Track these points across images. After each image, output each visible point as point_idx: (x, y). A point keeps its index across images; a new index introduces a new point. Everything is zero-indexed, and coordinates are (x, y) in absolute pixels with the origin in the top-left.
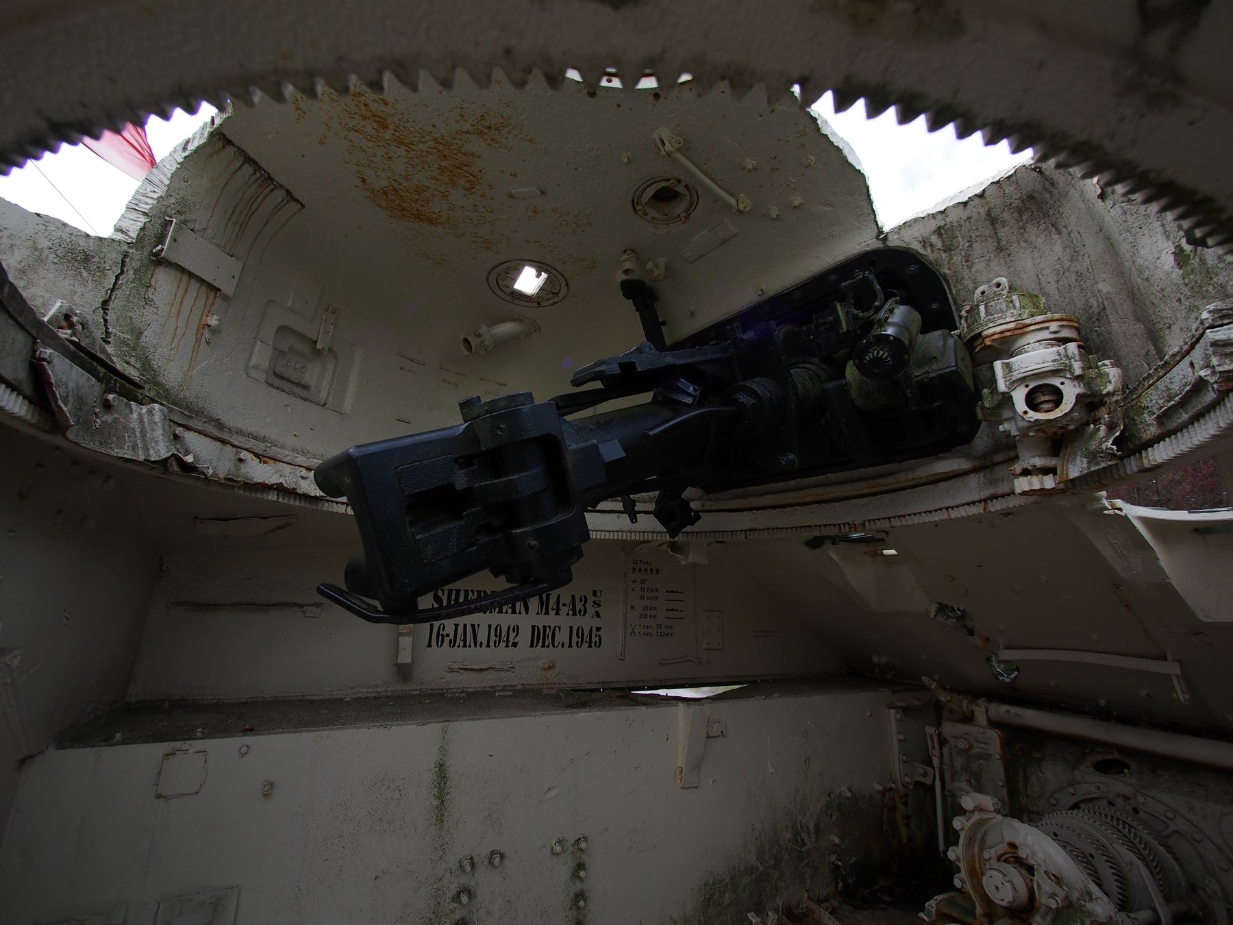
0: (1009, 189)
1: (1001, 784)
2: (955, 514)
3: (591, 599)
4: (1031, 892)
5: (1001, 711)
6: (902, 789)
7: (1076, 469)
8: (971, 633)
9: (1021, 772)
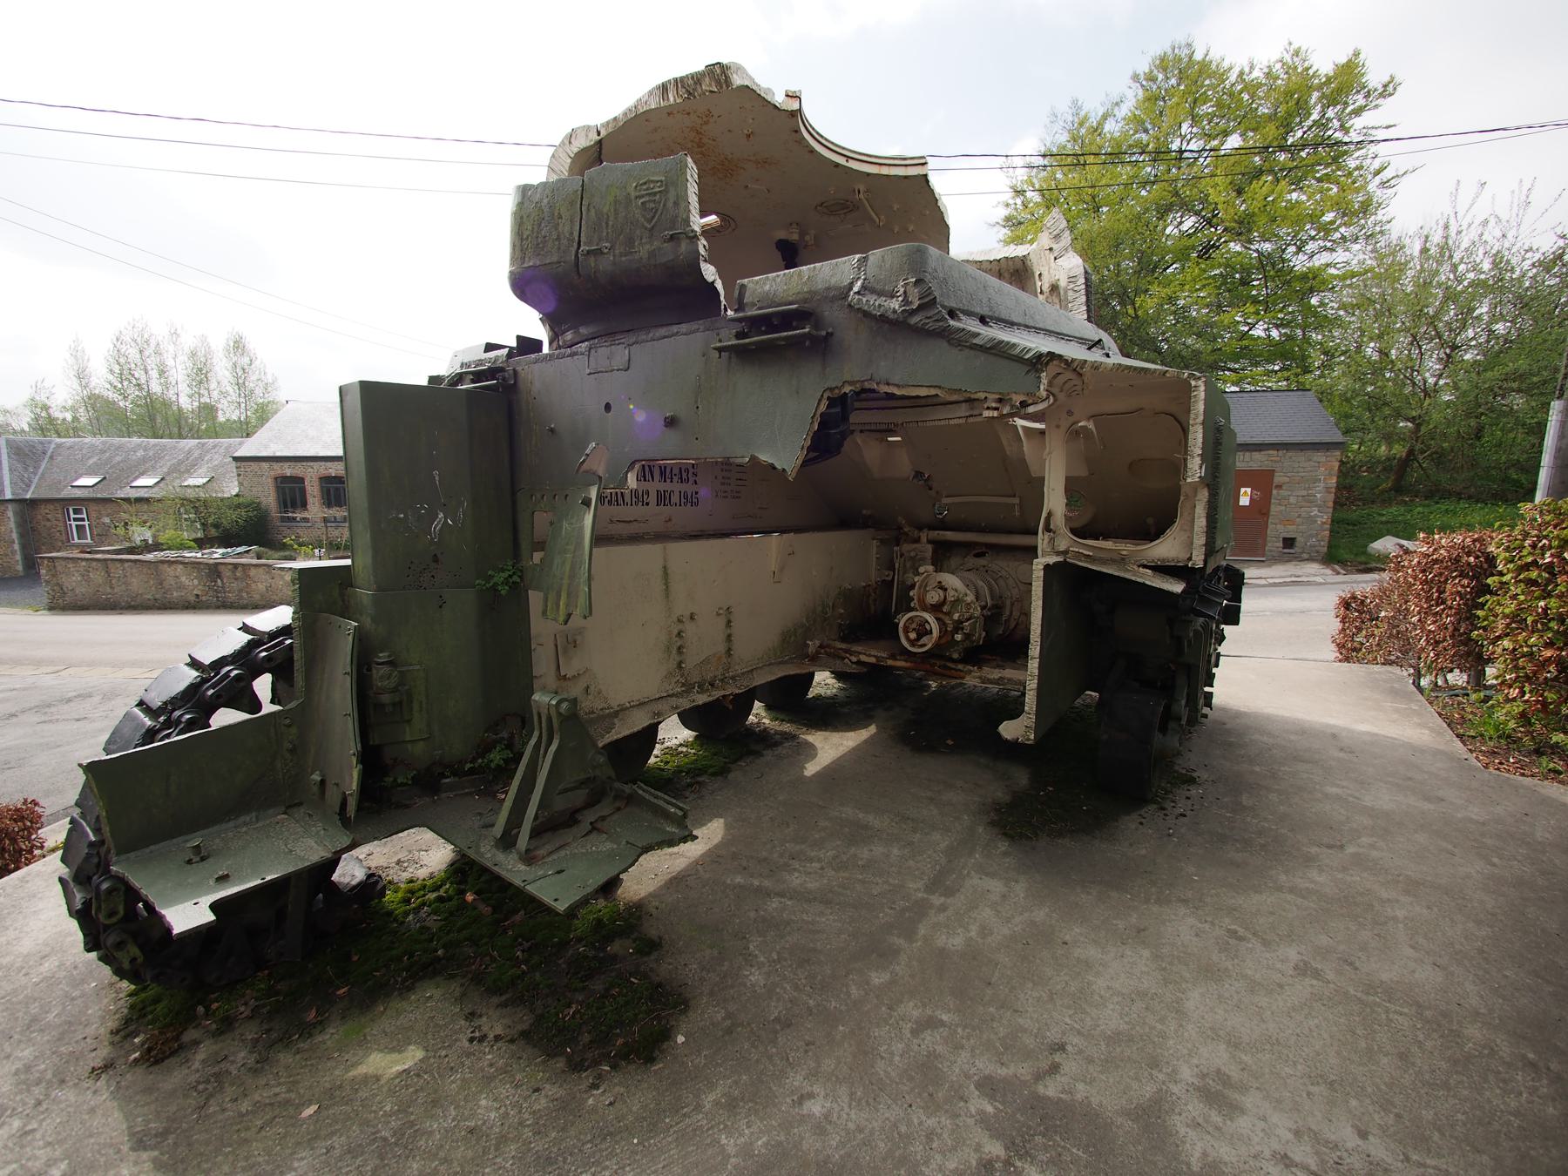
0: (1011, 263)
2: (951, 422)
3: (691, 470)
4: (945, 597)
5: (935, 534)
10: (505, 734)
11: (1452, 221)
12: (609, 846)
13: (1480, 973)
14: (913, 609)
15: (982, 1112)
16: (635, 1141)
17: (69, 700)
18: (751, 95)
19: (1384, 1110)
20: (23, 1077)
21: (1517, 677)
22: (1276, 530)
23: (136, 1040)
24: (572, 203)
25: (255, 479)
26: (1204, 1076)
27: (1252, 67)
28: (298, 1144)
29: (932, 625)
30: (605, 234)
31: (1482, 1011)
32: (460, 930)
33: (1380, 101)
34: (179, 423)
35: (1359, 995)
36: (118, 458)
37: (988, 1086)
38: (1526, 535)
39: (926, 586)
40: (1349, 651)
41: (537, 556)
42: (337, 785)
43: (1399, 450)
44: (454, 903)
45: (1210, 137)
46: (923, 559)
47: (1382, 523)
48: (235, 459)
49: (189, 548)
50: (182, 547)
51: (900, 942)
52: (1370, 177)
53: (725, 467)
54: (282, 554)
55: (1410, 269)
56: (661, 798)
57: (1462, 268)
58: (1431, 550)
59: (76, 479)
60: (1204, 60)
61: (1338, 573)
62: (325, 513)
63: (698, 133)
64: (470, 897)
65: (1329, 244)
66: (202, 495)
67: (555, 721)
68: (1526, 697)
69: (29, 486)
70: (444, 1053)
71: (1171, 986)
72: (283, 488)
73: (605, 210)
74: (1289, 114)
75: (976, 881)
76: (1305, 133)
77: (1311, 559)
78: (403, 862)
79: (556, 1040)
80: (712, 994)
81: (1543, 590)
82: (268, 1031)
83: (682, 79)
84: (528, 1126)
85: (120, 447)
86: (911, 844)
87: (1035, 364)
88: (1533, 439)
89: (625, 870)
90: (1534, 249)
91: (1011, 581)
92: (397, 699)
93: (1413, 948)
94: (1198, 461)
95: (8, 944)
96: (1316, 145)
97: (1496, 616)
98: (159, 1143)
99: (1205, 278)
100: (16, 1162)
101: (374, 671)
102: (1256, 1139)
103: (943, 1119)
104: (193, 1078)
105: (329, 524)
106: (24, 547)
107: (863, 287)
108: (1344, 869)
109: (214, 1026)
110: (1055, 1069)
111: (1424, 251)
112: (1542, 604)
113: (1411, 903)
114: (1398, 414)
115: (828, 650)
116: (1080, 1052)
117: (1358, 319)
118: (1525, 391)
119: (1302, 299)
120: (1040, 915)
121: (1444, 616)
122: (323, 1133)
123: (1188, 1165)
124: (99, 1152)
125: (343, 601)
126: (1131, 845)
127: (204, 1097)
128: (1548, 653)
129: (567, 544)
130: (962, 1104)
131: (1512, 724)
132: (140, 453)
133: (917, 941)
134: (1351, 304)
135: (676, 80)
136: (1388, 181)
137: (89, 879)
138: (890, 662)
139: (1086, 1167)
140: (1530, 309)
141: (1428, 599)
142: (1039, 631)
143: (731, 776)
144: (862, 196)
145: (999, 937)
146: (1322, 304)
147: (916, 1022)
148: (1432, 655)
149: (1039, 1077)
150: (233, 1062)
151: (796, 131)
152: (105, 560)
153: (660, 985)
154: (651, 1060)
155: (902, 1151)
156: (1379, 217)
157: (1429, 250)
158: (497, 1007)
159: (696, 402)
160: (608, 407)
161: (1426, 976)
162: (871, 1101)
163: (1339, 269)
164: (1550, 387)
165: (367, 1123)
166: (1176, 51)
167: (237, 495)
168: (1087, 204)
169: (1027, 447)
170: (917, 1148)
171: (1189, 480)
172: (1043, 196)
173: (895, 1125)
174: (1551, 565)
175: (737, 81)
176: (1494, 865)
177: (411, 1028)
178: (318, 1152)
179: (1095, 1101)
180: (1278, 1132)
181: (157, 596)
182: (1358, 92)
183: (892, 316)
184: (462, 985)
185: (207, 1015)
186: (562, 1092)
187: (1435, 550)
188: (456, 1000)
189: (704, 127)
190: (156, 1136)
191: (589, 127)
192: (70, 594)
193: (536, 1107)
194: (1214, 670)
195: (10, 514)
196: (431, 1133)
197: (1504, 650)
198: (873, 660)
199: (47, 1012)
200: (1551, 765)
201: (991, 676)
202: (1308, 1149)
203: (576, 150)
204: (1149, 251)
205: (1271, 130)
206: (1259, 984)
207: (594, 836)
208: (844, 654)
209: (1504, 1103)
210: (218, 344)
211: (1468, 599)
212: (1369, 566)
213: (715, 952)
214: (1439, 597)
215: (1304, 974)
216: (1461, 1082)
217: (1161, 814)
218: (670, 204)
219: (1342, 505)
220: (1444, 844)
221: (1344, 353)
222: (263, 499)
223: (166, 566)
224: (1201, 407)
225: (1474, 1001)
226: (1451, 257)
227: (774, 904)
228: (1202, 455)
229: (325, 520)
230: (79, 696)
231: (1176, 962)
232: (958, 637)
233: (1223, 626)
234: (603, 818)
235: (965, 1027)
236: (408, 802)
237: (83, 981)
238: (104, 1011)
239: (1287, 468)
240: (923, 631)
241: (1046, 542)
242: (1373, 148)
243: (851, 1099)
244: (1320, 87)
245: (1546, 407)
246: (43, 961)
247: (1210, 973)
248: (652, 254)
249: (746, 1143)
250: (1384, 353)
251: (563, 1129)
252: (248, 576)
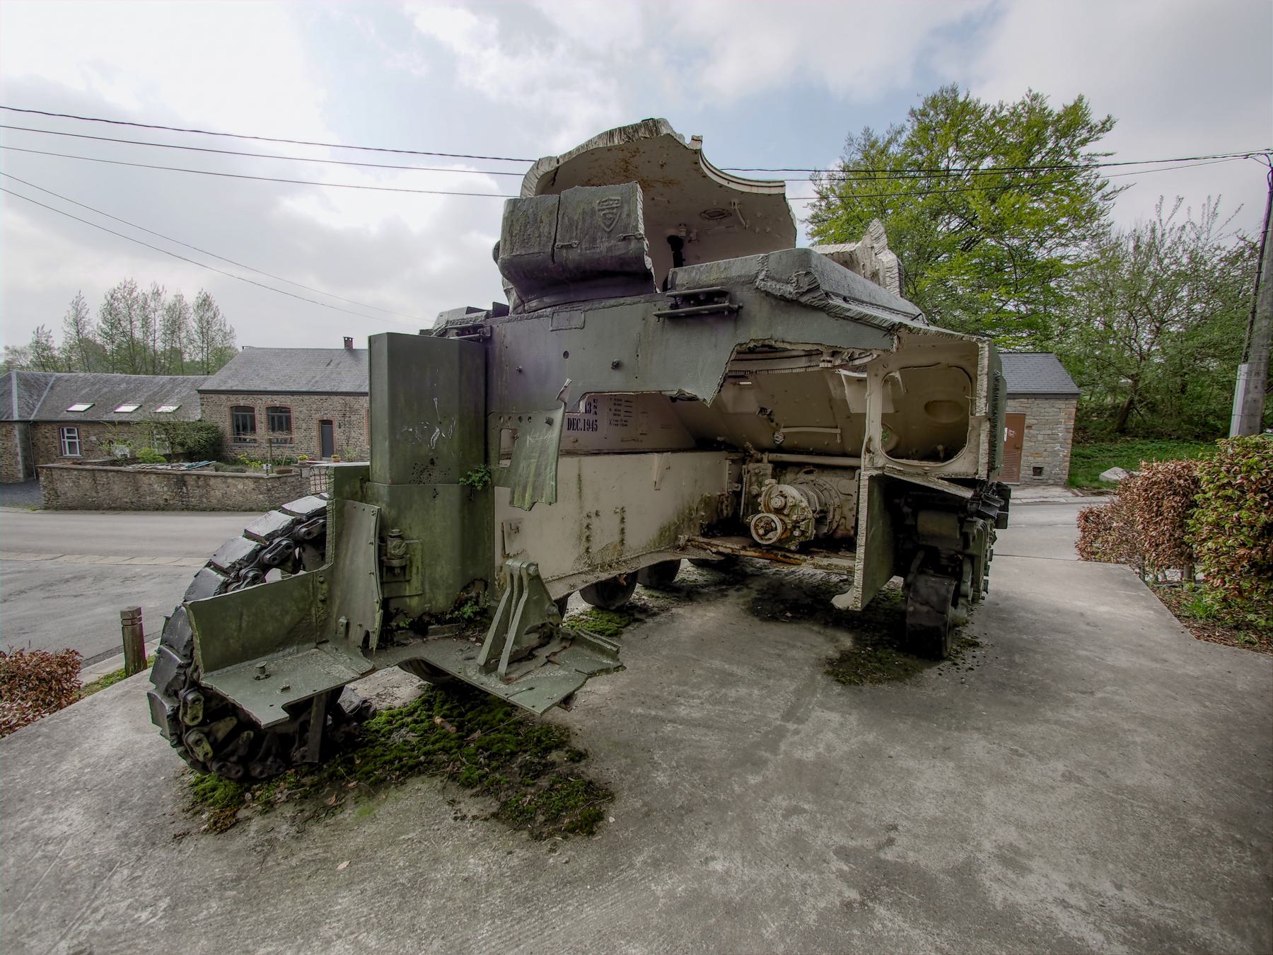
2: (794, 371)
3: (593, 404)
4: (786, 504)
5: (774, 456)
6: (727, 495)
7: (838, 362)
8: (772, 421)
10: (473, 594)
11: (1158, 226)
12: (562, 673)
13: (1199, 780)
14: (760, 512)
15: (840, 871)
16: (589, 887)
17: (67, 581)
18: (672, 141)
19: (1133, 871)
20: (123, 840)
21: (1219, 571)
22: (1028, 461)
23: (203, 816)
24: (551, 213)
25: (215, 408)
26: (1000, 848)
27: (1002, 108)
28: (339, 887)
29: (777, 523)
30: (574, 234)
31: (1201, 806)
32: (433, 744)
33: (1100, 135)
34: (154, 362)
35: (1111, 794)
36: (106, 390)
37: (843, 853)
38: (1222, 462)
39: (770, 495)
40: (1088, 552)
41: (505, 463)
42: (360, 625)
43: (1122, 400)
44: (426, 724)
45: (970, 159)
46: (765, 475)
47: (1110, 457)
48: (200, 392)
49: (159, 462)
50: (154, 461)
51: (767, 755)
52: (1093, 191)
53: (617, 402)
54: (234, 467)
55: (1127, 261)
56: (599, 639)
57: (1166, 261)
58: (1151, 474)
59: (71, 406)
60: (965, 101)
61: (1077, 496)
62: (270, 435)
63: (626, 162)
64: (438, 720)
65: (1063, 241)
66: (172, 419)
67: (525, 582)
68: (1227, 586)
69: (33, 410)
70: (436, 827)
71: (972, 787)
72: (237, 416)
73: (576, 218)
74: (1031, 144)
75: (818, 713)
76: (1043, 157)
77: (1055, 484)
78: (382, 695)
79: (520, 819)
80: (630, 789)
81: (1236, 504)
82: (302, 811)
83: (624, 128)
84: (507, 877)
85: (107, 381)
86: (767, 687)
87: (890, 330)
88: (1226, 394)
89: (578, 689)
90: (1222, 247)
91: (833, 493)
92: (404, 564)
93: (1149, 763)
94: (984, 401)
95: (90, 749)
96: (1051, 168)
97: (1202, 524)
98: (235, 886)
99: (969, 266)
100: (131, 897)
101: (389, 542)
102: (1041, 890)
103: (812, 875)
104: (251, 843)
105: (273, 445)
106: (25, 459)
107: (767, 276)
108: (1095, 708)
109: (260, 808)
110: (891, 842)
111: (1137, 247)
112: (1236, 514)
113: (1146, 732)
114: (1120, 372)
115: (693, 543)
116: (909, 831)
117: (1087, 298)
118: (1220, 357)
119: (1043, 283)
120: (870, 737)
121: (1162, 524)
122: (356, 880)
123: (994, 906)
124: (192, 891)
125: (362, 492)
126: (934, 689)
127: (262, 856)
128: (1241, 552)
129: (532, 452)
130: (825, 865)
131: (1216, 607)
132: (123, 386)
133: (779, 755)
134: (1081, 286)
135: (620, 129)
136: (1108, 195)
137: (176, 694)
138: (742, 552)
139: (920, 907)
140: (1220, 294)
141: (1150, 511)
142: (864, 526)
143: (624, 637)
144: (736, 207)
145: (841, 753)
146: (1059, 287)
147: (785, 810)
148: (1154, 555)
149: (880, 847)
150: (279, 832)
151: (696, 163)
152: (93, 470)
153: (590, 782)
154: (591, 833)
155: (784, 895)
156: (1102, 222)
157: (1140, 247)
158: (471, 796)
159: (637, 352)
160: (566, 354)
161: (1159, 782)
162: (758, 862)
163: (1071, 260)
164: (1237, 354)
165: (388, 874)
166: (944, 94)
167: (200, 421)
168: (876, 207)
169: (848, 391)
170: (796, 894)
171: (977, 415)
172: (842, 201)
173: (778, 878)
174: (1241, 485)
175: (664, 131)
176: (1206, 707)
177: (409, 810)
178: (355, 893)
179: (922, 863)
180: (1057, 885)
181: (134, 500)
182: (1083, 128)
183: (788, 296)
184: (442, 781)
185: (253, 799)
186: (529, 855)
187: (1154, 474)
188: (439, 791)
189: (631, 159)
190: (232, 881)
191: (551, 157)
192: (62, 497)
193: (511, 864)
194: (989, 563)
195: (16, 432)
196: (437, 880)
197: (1208, 550)
198: (730, 551)
199: (132, 797)
200: (1247, 638)
201: (820, 563)
202: (1080, 896)
203: (541, 173)
204: (926, 244)
205: (1018, 155)
206: (1037, 786)
207: (549, 666)
208: (706, 547)
209: (1220, 867)
210: (191, 299)
211: (1180, 512)
212: (1100, 490)
213: (629, 761)
214: (1158, 510)
215: (1070, 780)
216: (1188, 853)
217: (954, 668)
218: (624, 216)
219: (1079, 442)
220: (1168, 692)
221: (1077, 325)
222: (220, 424)
223: (142, 475)
224: (986, 362)
225: (1195, 799)
226: (1158, 253)
227: (669, 728)
228: (986, 397)
229: (270, 441)
230: (75, 577)
231: (974, 771)
232: (797, 533)
233: (994, 530)
234: (555, 654)
235: (822, 813)
236: (405, 642)
237: (154, 776)
238: (174, 796)
239: (1036, 412)
240: (769, 528)
241: (867, 460)
242: (1096, 171)
243: (743, 861)
244: (1054, 123)
245: (1235, 368)
246: (120, 761)
247: (999, 778)
248: (609, 249)
249: (670, 889)
250: (1108, 326)
251: (534, 879)
252: (208, 485)
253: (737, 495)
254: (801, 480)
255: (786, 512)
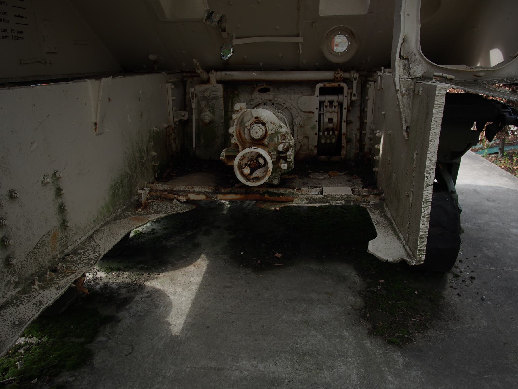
1: (222, 109)
4: (266, 130)
8: (224, 30)
9: (230, 101)
142: (435, 159)
198: (202, 197)
208: (171, 196)
253: (185, 124)
254: (258, 100)
255: (266, 142)
